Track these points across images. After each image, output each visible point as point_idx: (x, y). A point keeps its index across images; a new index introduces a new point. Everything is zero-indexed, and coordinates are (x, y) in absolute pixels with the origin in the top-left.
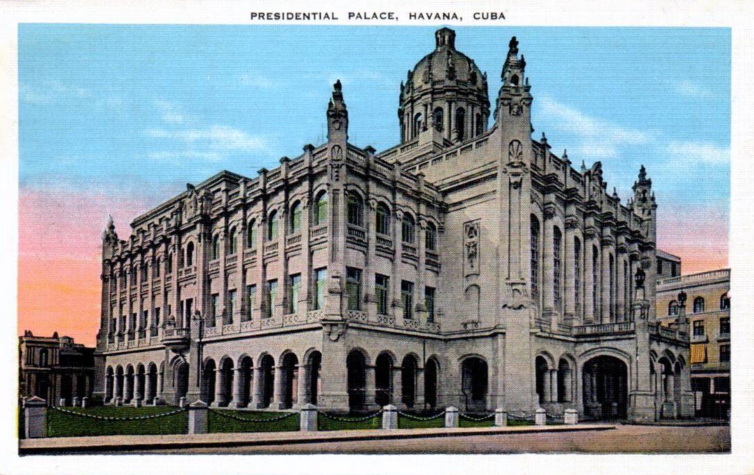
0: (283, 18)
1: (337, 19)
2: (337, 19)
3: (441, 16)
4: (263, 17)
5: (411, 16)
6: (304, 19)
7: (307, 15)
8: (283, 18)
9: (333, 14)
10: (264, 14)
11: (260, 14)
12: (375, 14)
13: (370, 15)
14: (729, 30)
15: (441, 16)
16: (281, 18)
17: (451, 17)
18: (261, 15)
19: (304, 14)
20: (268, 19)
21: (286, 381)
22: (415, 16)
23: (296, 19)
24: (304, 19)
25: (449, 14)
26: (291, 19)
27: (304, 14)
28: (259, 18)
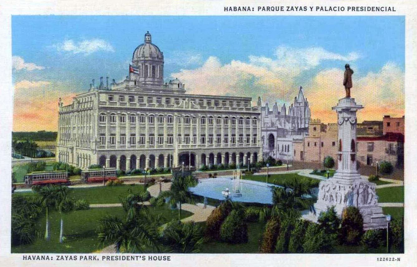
0: (365, 11)
1: (395, 11)
2: (395, 11)
3: (242, 9)
4: (354, 9)
5: (225, 9)
6: (376, 11)
7: (57, 257)
8: (365, 11)
9: (393, 7)
10: (92, 257)
11: (107, 257)
12: (330, 7)
13: (328, 8)
14: (12, 252)
15: (242, 9)
16: (119, 259)
17: (247, 9)
18: (353, 9)
19: (377, 8)
20: (112, 260)
21: (225, 246)
22: (227, 9)
23: (127, 260)
24: (376, 11)
25: (227, 8)
26: (370, 11)
27: (377, 8)
28: (107, 260)
